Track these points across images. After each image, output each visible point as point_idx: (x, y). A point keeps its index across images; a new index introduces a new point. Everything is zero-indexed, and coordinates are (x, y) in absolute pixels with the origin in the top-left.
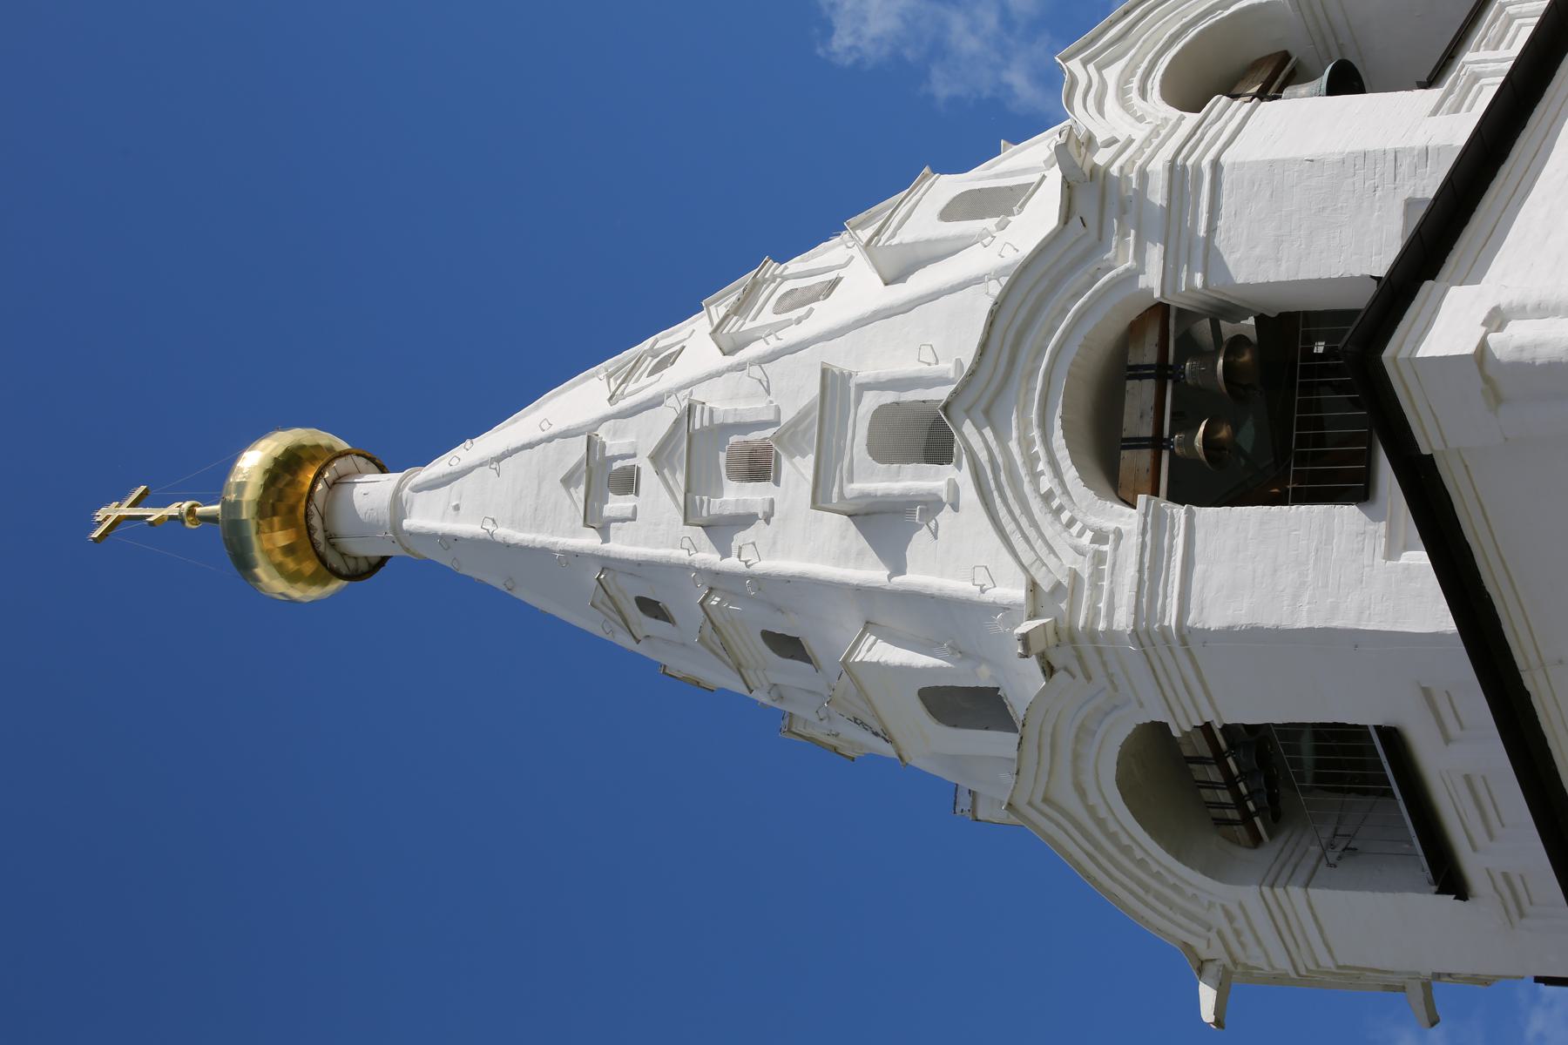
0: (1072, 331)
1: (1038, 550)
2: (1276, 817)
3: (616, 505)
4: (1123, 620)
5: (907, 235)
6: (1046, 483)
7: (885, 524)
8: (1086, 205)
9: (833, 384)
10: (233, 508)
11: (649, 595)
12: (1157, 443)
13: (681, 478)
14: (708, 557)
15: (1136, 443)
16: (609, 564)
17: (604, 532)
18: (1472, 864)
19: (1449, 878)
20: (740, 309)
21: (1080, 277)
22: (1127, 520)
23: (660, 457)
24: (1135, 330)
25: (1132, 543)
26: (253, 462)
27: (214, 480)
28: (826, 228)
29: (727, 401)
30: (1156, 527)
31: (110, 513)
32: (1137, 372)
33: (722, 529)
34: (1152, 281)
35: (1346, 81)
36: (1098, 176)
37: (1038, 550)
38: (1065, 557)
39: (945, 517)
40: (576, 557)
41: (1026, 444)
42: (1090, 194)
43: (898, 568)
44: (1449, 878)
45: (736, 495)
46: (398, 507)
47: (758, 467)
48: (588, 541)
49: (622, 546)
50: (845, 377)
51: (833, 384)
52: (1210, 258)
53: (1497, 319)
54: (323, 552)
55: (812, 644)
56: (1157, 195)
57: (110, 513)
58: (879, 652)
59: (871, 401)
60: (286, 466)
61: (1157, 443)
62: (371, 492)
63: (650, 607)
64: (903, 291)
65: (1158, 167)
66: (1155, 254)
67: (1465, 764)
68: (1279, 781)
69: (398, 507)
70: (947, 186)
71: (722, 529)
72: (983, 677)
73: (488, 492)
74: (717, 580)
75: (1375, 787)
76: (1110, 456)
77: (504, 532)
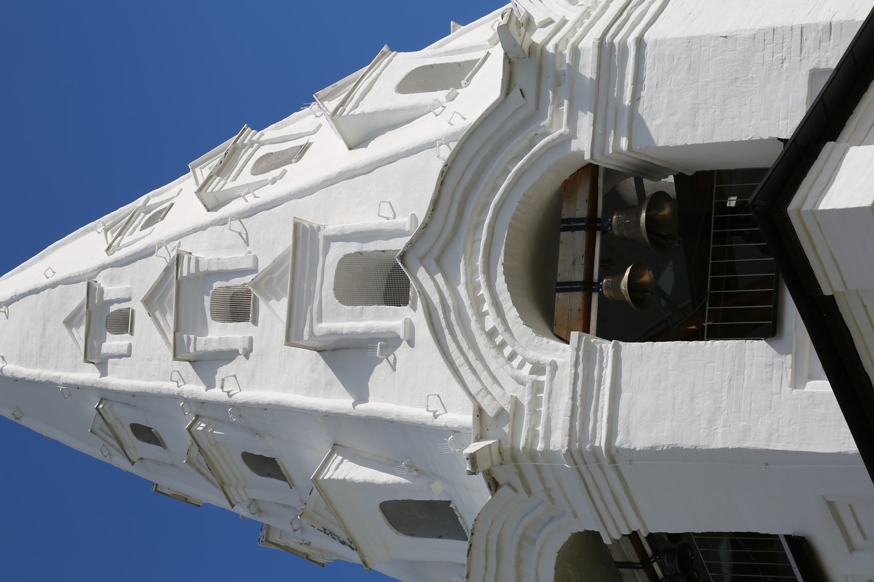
0: (513, 189)
3: (113, 343)
4: (559, 441)
6: (491, 321)
7: (350, 358)
9: (304, 237)
11: (142, 422)
12: (587, 286)
13: (170, 319)
14: (195, 388)
15: (569, 287)
16: (106, 395)
17: (102, 366)
20: (222, 170)
21: (520, 142)
22: (561, 354)
24: (568, 188)
25: (565, 374)
28: (299, 100)
29: (211, 251)
30: (587, 361)
32: (570, 225)
33: (206, 364)
34: (583, 144)
36: (536, 54)
37: (483, 378)
38: (507, 387)
40: (77, 389)
41: (473, 288)
43: (362, 396)
45: (219, 334)
48: (89, 375)
49: (119, 379)
50: (315, 231)
51: (304, 237)
52: (635, 123)
55: (286, 464)
56: (588, 69)
58: (345, 470)
59: (338, 251)
61: (587, 286)
63: (143, 433)
65: (589, 44)
66: (585, 121)
70: (403, 63)
72: (437, 492)
74: (203, 408)
76: (547, 298)
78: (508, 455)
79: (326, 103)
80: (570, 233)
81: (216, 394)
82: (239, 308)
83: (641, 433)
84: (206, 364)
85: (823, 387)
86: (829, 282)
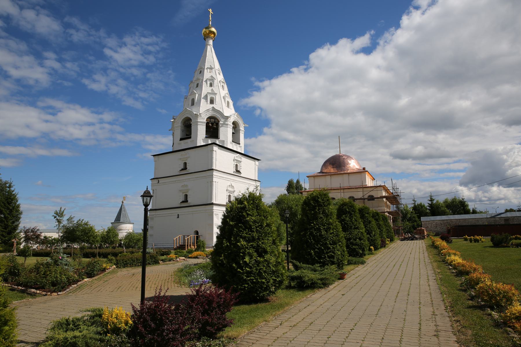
1: (204, 111)
2: (185, 126)
4: (199, 120)
7: (206, 97)
9: (216, 94)
10: (210, 28)
11: (201, 72)
14: (204, 80)
16: (204, 69)
18: (182, 141)
19: (181, 139)
22: (205, 121)
23: (214, 109)
24: (218, 120)
26: (213, 29)
28: (229, 90)
30: (204, 123)
31: (211, 10)
33: (206, 81)
34: (221, 122)
35: (233, 133)
37: (204, 111)
38: (202, 115)
42: (227, 118)
44: (181, 139)
45: (209, 83)
46: (209, 45)
47: (211, 85)
48: (206, 67)
49: (205, 70)
51: (216, 94)
52: (222, 126)
54: (206, 37)
57: (211, 10)
58: (197, 95)
60: (214, 33)
62: (211, 42)
63: (201, 71)
67: (187, 144)
68: (188, 127)
69: (209, 45)
72: (195, 104)
74: (203, 80)
75: (187, 135)
76: (210, 118)
80: (143, 228)
81: (204, 83)
84: (206, 81)
85: (487, 224)
86: (414, 190)
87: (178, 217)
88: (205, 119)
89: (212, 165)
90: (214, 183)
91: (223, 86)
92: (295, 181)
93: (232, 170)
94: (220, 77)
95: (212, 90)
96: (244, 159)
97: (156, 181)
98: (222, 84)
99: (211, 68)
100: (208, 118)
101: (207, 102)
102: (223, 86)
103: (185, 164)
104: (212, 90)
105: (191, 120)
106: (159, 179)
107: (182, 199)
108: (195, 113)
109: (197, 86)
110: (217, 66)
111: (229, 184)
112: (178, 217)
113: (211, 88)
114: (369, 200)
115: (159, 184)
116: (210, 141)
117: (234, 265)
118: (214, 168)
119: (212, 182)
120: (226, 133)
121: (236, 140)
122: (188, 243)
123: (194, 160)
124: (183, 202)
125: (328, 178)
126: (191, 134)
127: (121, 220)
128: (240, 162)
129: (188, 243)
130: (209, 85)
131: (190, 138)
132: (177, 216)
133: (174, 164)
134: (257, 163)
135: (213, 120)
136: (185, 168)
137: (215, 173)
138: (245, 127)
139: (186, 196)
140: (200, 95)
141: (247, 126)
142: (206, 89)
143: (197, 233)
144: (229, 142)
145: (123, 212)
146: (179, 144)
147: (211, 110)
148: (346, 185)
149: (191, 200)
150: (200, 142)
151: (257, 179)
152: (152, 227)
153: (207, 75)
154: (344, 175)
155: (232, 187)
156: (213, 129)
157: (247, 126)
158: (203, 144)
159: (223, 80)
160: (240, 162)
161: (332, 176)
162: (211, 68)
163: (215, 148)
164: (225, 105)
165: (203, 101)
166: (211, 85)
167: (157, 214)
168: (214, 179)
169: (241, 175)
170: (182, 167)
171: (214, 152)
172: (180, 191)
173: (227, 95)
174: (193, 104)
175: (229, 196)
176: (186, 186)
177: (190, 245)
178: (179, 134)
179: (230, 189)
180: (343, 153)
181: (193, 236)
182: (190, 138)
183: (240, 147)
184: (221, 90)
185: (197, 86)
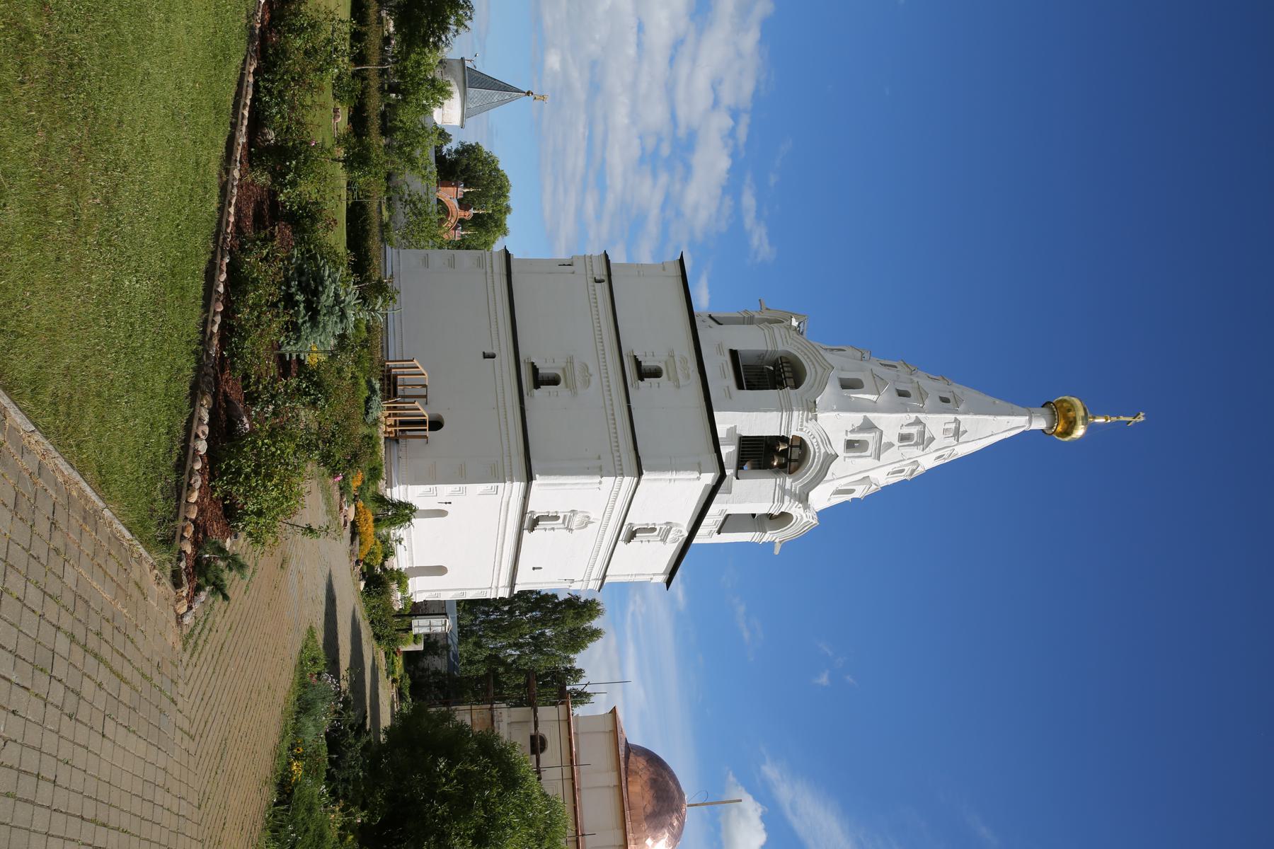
1: (825, 425)
2: (775, 364)
4: (795, 414)
5: (862, 487)
7: (868, 426)
8: (803, 496)
11: (946, 403)
12: (792, 446)
14: (921, 416)
16: (956, 412)
18: (727, 358)
19: (734, 354)
20: (913, 471)
23: (830, 458)
24: (797, 469)
26: (1079, 432)
27: (1091, 429)
28: (886, 489)
29: (914, 452)
31: (1141, 418)
33: (918, 422)
34: (789, 481)
35: (754, 515)
36: (800, 502)
37: (825, 425)
38: (811, 424)
39: (850, 428)
42: (803, 499)
44: (734, 354)
45: (914, 430)
48: (960, 417)
49: (951, 417)
53: (699, 478)
54: (1062, 414)
55: (895, 394)
56: (787, 498)
57: (1141, 418)
58: (873, 397)
59: (868, 453)
60: (1067, 432)
62: (1040, 424)
64: (847, 479)
68: (768, 375)
70: (856, 495)
71: (918, 422)
73: (989, 428)
76: (802, 444)
77: (991, 418)
78: (809, 410)
79: (444, 670)
81: (913, 416)
82: (904, 438)
83: (775, 415)
87: (486, 356)
88: (799, 434)
89: (653, 469)
90: (597, 479)
91: (902, 471)
92: (596, 623)
93: (635, 519)
94: (928, 461)
95: (891, 445)
96: (671, 549)
97: (600, 272)
98: (908, 470)
99: (957, 433)
100: (802, 440)
101: (853, 431)
102: (902, 471)
103: (656, 373)
104: (891, 445)
105: (797, 385)
106: (605, 284)
107: (545, 369)
108: (818, 400)
109: (903, 394)
110: (963, 450)
111: (593, 517)
112: (486, 356)
113: (895, 440)
114: (533, 738)
115: (591, 281)
116: (729, 451)
117: (1100, 420)
118: (538, 481)
119: (601, 471)
120: (754, 493)
121: (729, 523)
122: (404, 409)
123: (666, 404)
124: (535, 370)
125: (611, 779)
126: (751, 387)
127: (471, 91)
128: (664, 540)
129: (404, 409)
130: (906, 431)
131: (740, 387)
132: (488, 351)
133: (657, 336)
134: (661, 579)
135: (795, 453)
136: (644, 373)
137: (628, 481)
138: (772, 544)
139: (554, 381)
140: (874, 408)
141: (777, 551)
142: (891, 423)
143: (436, 425)
144: (724, 507)
145: (497, 96)
146: (720, 347)
147: (830, 451)
148: (584, 780)
149: (539, 399)
150: (726, 422)
151: (607, 580)
152: (452, 263)
153: (937, 423)
154: (619, 833)
155: (587, 522)
156: (763, 454)
157: (777, 551)
158: (721, 432)
159: (920, 470)
160: (664, 540)
161: (616, 790)
162: (957, 433)
163: (709, 478)
164: (841, 484)
165: (857, 418)
166: (904, 438)
167: (496, 277)
168: (608, 481)
169: (526, 532)
170: (647, 363)
171: (696, 474)
172: (571, 361)
173: (874, 487)
174: (847, 385)
175: (557, 518)
176: (587, 383)
177: (395, 415)
178: (753, 341)
179: (577, 520)
180: (690, 814)
181: (425, 413)
182: (740, 387)
183: (710, 534)
184: (890, 469)
185: (903, 394)
